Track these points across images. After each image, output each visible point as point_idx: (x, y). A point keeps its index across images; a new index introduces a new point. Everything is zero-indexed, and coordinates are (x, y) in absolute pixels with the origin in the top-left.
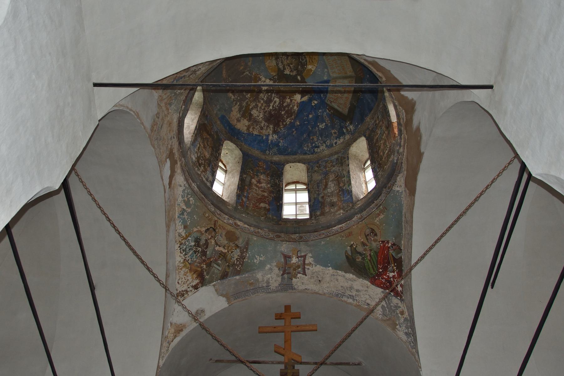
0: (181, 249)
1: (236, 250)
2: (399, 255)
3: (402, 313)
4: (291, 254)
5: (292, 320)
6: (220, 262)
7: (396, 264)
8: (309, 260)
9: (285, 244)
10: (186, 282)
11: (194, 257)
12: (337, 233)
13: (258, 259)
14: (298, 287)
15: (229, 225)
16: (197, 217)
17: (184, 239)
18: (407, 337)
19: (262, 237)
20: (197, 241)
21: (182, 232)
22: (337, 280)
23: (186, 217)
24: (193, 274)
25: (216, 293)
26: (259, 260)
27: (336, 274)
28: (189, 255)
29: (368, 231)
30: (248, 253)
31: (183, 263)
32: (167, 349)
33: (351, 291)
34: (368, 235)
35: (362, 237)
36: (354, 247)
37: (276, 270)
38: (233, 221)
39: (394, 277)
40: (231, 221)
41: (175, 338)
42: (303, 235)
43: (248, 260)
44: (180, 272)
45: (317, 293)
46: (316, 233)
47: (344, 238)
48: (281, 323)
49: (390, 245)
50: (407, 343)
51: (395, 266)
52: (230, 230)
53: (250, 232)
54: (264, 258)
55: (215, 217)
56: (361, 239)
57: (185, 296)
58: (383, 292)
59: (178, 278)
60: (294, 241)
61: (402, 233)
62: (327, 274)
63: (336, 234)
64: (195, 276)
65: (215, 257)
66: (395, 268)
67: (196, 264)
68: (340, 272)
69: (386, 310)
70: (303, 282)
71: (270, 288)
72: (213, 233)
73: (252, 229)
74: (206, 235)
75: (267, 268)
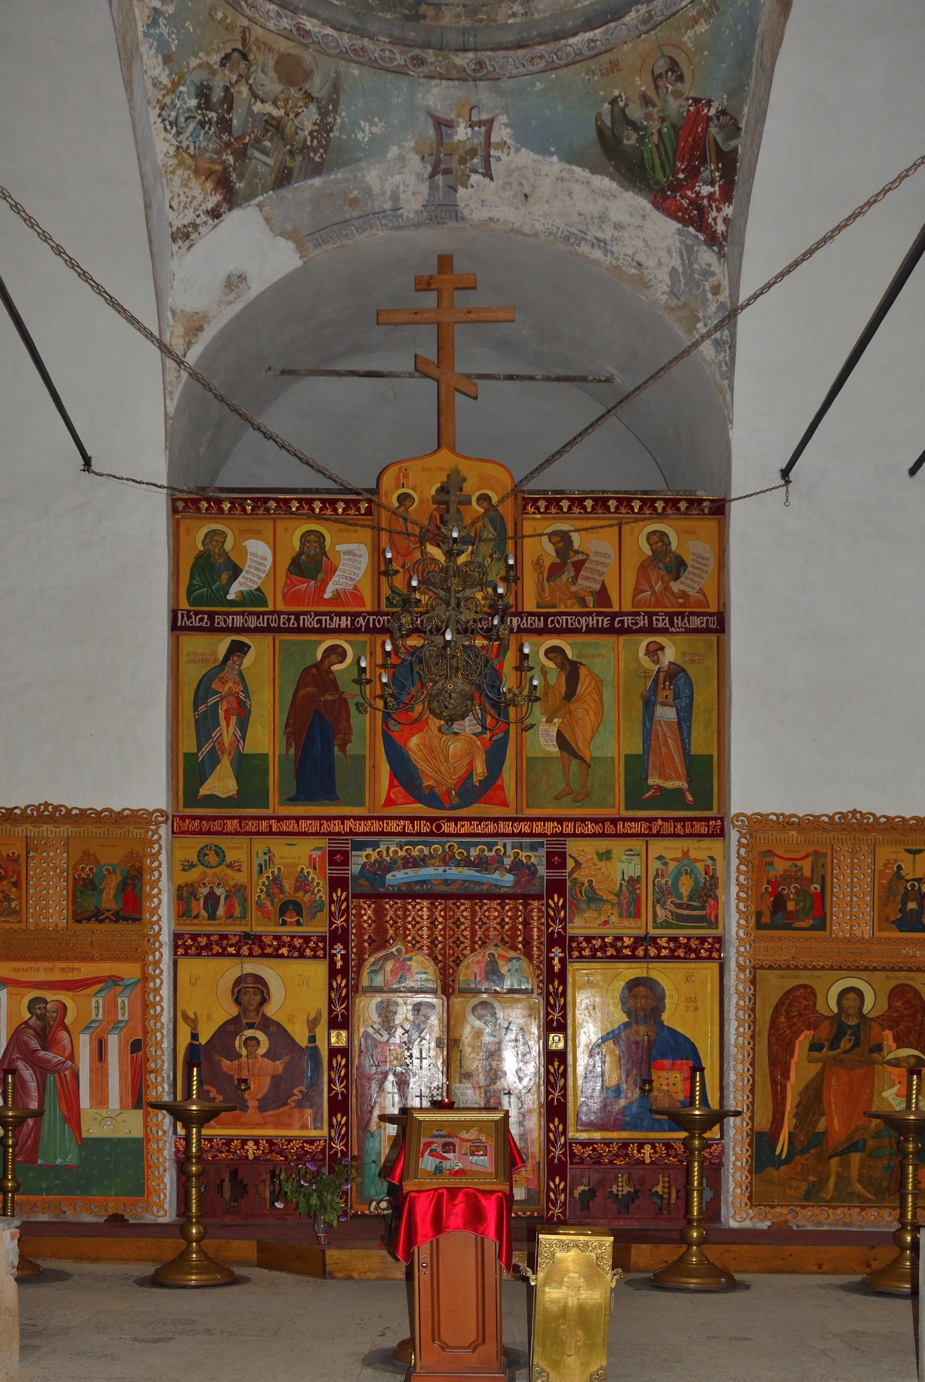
0: (164, 120)
1: (306, 107)
2: (732, 144)
3: (716, 290)
4: (453, 117)
5: (457, 294)
6: (267, 144)
7: (720, 165)
8: (501, 133)
9: (437, 85)
10: (191, 202)
11: (201, 138)
12: (578, 58)
13: (367, 131)
14: (471, 214)
15: (283, 37)
16: (193, 26)
17: (168, 93)
18: (717, 351)
19: (375, 65)
20: (203, 93)
21: (160, 75)
22: (570, 194)
23: (165, 30)
24: (204, 182)
25: (266, 228)
26: (370, 132)
27: (566, 175)
28: (188, 134)
29: (661, 65)
30: (340, 116)
31: (176, 156)
32: (175, 374)
33: (604, 226)
34: (660, 76)
35: (643, 78)
36: (622, 104)
37: (415, 162)
38: (293, 19)
39: (711, 196)
40: (286, 23)
41: (189, 348)
42: (488, 57)
43: (341, 134)
44: (171, 180)
45: (518, 232)
46: (521, 52)
47: (596, 78)
48: (429, 300)
49: (712, 112)
50: (713, 366)
51: (718, 169)
52: (287, 52)
53: (341, 51)
54: (383, 127)
55: (241, 17)
56: (641, 86)
57: (193, 237)
58: (679, 232)
59: (168, 195)
60: (462, 76)
61: (748, 85)
62: (547, 175)
63: (574, 63)
64: (209, 185)
65: (253, 132)
66: (717, 174)
67: (208, 155)
68: (578, 170)
69: (680, 282)
70: (483, 197)
71: (401, 216)
72: (242, 66)
73: (345, 39)
74: (224, 75)
75: (390, 155)
